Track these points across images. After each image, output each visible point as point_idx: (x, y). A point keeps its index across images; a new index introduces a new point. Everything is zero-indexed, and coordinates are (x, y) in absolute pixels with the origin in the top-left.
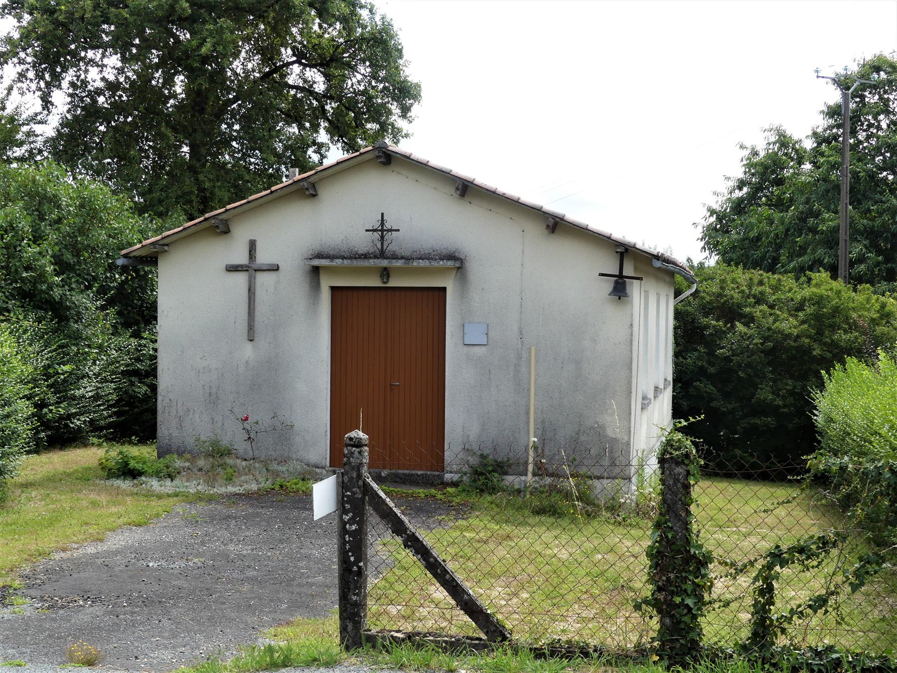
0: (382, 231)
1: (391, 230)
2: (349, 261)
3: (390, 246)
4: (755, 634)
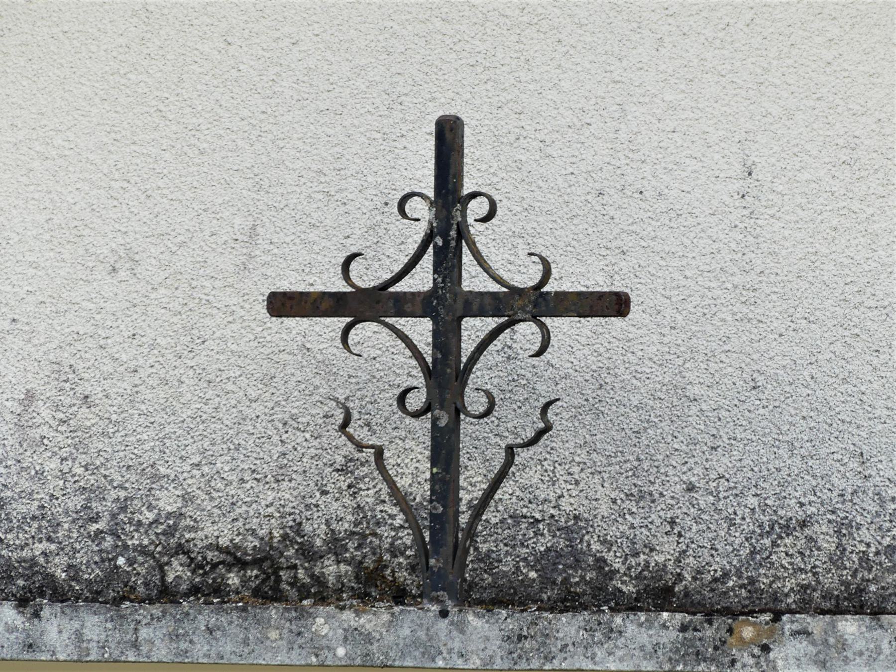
0: (446, 306)
1: (538, 303)
2: (94, 625)
3: (529, 473)
4: (585, 609)
